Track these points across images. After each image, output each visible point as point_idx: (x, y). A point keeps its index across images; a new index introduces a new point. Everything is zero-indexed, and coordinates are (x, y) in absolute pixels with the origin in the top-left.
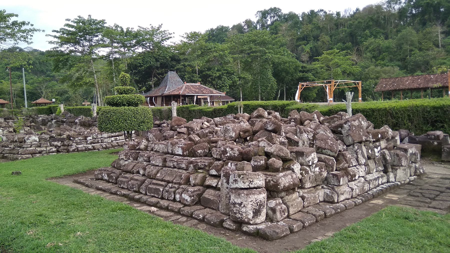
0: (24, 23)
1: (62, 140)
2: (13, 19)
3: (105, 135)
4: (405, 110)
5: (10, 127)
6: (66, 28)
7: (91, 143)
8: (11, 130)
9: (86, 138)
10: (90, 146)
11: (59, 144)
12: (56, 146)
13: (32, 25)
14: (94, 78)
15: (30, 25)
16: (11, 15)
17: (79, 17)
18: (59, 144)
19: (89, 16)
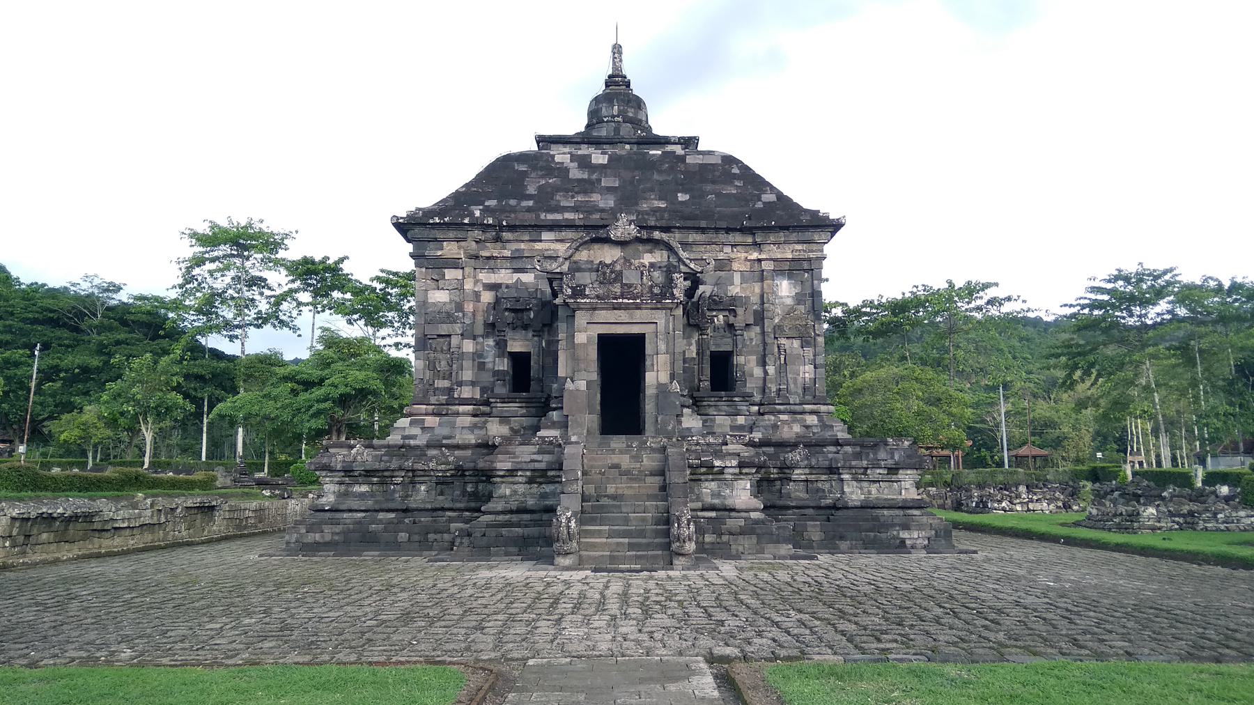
0: (1009, 299)
1: (1183, 516)
2: (991, 293)
3: (1242, 513)
4: (236, 439)
5: (1058, 499)
6: (1093, 296)
7: (1224, 522)
8: (1060, 504)
9: (1215, 515)
10: (1222, 527)
11: (1181, 520)
12: (1178, 523)
13: (1024, 301)
14: (1153, 401)
15: (1020, 301)
16: (986, 286)
17: (1120, 271)
18: (1181, 520)
19: (1140, 264)
